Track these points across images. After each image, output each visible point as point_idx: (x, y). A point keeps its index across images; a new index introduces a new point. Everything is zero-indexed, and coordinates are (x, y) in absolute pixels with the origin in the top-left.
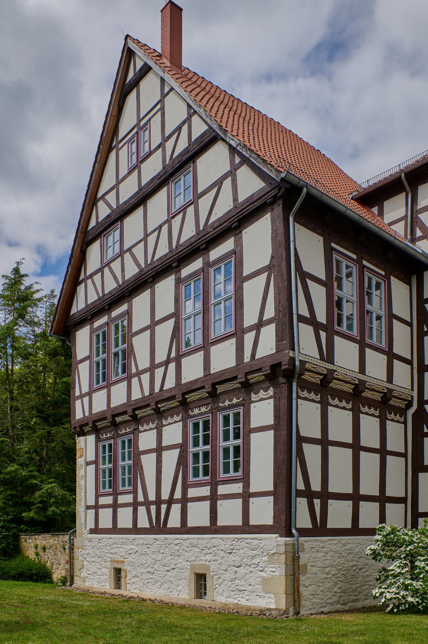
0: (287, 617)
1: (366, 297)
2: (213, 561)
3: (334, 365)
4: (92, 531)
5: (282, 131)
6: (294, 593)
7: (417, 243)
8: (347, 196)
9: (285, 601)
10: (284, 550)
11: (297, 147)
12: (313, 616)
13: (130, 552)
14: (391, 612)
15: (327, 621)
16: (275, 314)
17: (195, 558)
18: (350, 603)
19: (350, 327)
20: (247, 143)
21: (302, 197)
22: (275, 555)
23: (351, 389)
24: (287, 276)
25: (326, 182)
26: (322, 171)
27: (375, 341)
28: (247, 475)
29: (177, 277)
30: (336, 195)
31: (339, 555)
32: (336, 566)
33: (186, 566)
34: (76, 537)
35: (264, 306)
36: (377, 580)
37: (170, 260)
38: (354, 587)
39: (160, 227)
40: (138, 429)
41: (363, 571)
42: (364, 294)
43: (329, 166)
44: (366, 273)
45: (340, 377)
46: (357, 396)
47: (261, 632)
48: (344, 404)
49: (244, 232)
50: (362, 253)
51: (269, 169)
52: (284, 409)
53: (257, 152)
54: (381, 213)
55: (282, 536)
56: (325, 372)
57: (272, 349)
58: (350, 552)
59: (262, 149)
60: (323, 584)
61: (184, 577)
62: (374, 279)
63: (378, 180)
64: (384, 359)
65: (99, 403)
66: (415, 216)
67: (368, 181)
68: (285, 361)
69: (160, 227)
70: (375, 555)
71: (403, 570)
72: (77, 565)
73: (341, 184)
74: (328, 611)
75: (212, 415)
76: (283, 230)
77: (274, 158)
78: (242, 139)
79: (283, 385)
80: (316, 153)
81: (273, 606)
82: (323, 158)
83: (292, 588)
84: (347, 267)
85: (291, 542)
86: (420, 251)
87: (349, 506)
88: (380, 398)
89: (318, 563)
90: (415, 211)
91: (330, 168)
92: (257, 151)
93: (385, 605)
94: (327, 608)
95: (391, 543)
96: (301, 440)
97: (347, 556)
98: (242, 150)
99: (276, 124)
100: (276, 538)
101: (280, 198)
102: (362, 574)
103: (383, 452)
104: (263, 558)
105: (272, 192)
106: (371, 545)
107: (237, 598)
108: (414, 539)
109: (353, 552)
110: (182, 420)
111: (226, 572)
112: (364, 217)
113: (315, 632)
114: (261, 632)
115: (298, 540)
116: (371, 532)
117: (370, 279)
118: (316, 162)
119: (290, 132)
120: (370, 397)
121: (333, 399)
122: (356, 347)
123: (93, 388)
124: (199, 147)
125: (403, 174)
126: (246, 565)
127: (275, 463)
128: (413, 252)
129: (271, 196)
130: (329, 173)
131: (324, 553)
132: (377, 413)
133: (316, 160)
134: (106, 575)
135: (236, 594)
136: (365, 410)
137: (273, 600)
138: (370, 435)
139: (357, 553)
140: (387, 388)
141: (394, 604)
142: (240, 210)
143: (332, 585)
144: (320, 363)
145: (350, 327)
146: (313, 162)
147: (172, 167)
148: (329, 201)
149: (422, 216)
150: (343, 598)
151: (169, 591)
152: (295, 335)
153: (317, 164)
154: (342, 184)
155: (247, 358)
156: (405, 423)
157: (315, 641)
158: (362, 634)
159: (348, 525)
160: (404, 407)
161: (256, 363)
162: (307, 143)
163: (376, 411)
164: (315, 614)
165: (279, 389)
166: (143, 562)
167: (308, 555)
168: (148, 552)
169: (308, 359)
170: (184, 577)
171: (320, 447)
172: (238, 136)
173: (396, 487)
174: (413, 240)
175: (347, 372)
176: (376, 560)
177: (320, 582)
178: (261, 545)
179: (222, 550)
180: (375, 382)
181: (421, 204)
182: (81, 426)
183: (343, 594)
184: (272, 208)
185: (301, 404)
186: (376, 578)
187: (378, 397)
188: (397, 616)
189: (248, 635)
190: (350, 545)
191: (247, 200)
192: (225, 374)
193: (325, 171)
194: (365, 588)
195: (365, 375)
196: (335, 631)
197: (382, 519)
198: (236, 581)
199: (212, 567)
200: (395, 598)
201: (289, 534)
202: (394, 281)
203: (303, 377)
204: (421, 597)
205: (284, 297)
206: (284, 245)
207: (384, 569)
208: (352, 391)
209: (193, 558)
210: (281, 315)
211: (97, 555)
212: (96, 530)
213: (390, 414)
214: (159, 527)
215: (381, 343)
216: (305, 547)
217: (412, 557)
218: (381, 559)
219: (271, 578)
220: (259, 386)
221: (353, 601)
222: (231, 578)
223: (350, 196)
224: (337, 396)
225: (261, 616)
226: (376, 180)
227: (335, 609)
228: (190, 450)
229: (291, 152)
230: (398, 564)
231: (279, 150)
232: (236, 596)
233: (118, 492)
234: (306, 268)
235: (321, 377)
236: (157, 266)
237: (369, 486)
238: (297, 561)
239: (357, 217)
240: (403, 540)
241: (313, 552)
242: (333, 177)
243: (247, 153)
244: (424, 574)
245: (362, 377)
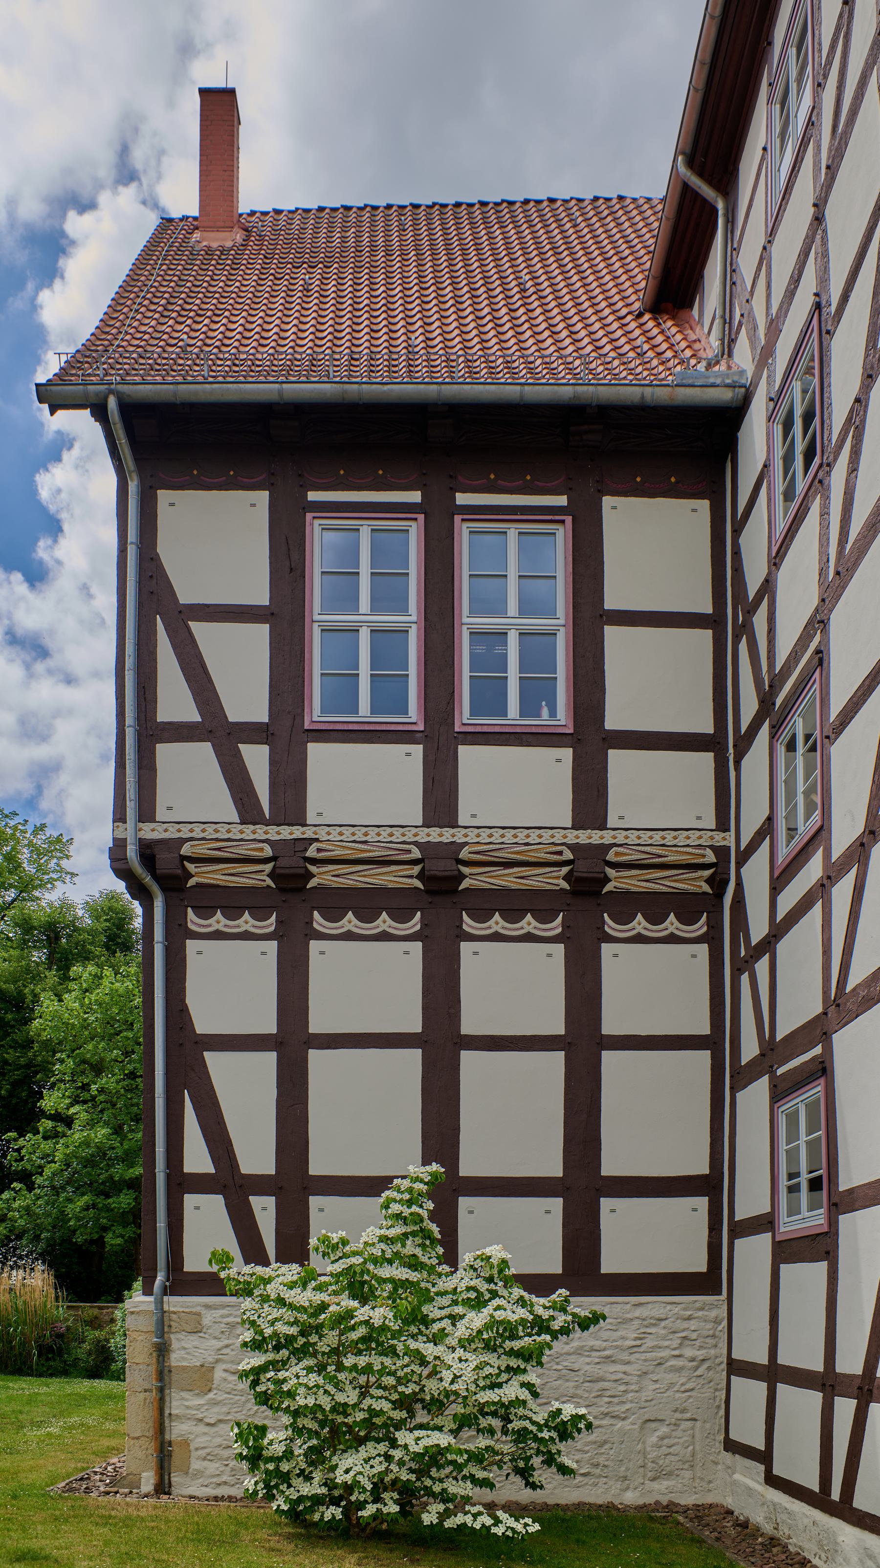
23: (411, 877)
48: (384, 923)
88: (704, 884)
120: (514, 886)
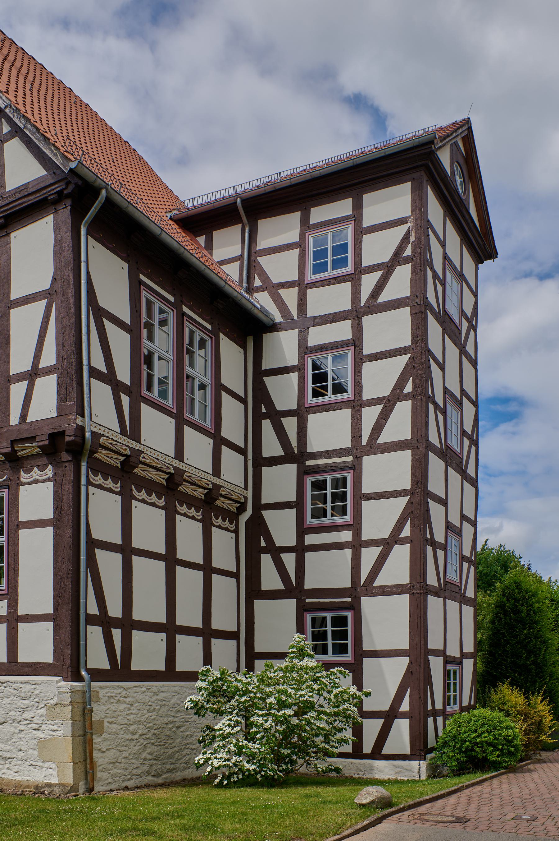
0: (75, 796)
1: (186, 357)
3: (140, 444)
5: (75, 103)
6: (85, 760)
7: (255, 295)
8: (163, 214)
9: (72, 773)
10: (70, 700)
11: (96, 130)
12: (113, 794)
14: (220, 785)
15: (133, 800)
16: (57, 361)
18: (165, 773)
19: (163, 394)
20: (20, 107)
21: (100, 202)
22: (56, 707)
23: (163, 479)
24: (75, 310)
25: (136, 189)
26: (136, 176)
27: (197, 418)
28: (14, 590)
30: (143, 205)
31: (148, 707)
32: (145, 723)
35: (40, 347)
36: (200, 742)
38: (170, 752)
41: (182, 729)
42: (183, 352)
43: (141, 168)
44: (186, 323)
45: (148, 461)
46: (171, 489)
47: (36, 818)
49: (13, 235)
50: (181, 296)
51: (53, 151)
52: (68, 498)
53: (35, 123)
54: (209, 246)
55: (66, 679)
56: (128, 452)
57: (51, 411)
58: (164, 703)
59: (44, 119)
60: (127, 748)
62: (198, 333)
63: (207, 201)
64: (209, 444)
66: (253, 258)
67: (193, 199)
68: (70, 430)
70: (198, 709)
71: (233, 729)
73: (157, 195)
74: (135, 785)
76: (71, 243)
77: (61, 139)
78: (13, 100)
79: (66, 464)
80: (124, 145)
81: (55, 781)
82: (133, 154)
83: (82, 754)
84: (161, 311)
85: (80, 689)
86: (259, 306)
87: (162, 640)
88: (203, 496)
89: (120, 718)
90: (253, 251)
91: (142, 170)
92: (36, 122)
93: (212, 776)
94: (133, 781)
95: (220, 693)
96: (94, 544)
97: (159, 710)
98: (14, 116)
99: (67, 91)
100: (58, 682)
101: (68, 196)
102: (181, 734)
103: (207, 569)
104: (39, 711)
105: (57, 186)
106: (192, 695)
108: (250, 688)
109: (168, 703)
112: (186, 247)
113: (114, 816)
114: (36, 818)
115: (89, 686)
116: (192, 677)
117: (192, 333)
118: (123, 158)
119: (88, 107)
120: (190, 493)
121: (140, 491)
122: (171, 422)
125: (239, 200)
126: (14, 720)
127: (55, 575)
128: (249, 306)
129: (55, 191)
130: (141, 177)
131: (128, 704)
132: (199, 516)
133: (123, 155)
136: (183, 510)
137: (54, 772)
138: (189, 545)
139: (174, 705)
140: (213, 483)
141: (224, 774)
142: (7, 202)
143: (139, 749)
144: (121, 439)
145: (163, 394)
146: (118, 156)
148: (137, 215)
149: (262, 260)
150: (154, 767)
152: (86, 395)
153: (123, 161)
154: (158, 196)
155: (15, 419)
156: (236, 532)
157: (114, 828)
158: (179, 816)
159: (161, 666)
160: (235, 511)
161: (27, 427)
162: (111, 128)
163: (198, 512)
164: (117, 790)
165: (61, 469)
167: (105, 708)
169: (104, 431)
171: (120, 556)
172: (7, 92)
173: (224, 618)
174: (250, 290)
175: (172, 462)
176: (199, 716)
177: (123, 746)
178: (36, 692)
180: (197, 472)
181: (262, 244)
183: (155, 762)
184: (55, 209)
185: (93, 494)
186: (199, 740)
187: (200, 494)
188: (228, 790)
189: (16, 823)
190: (164, 695)
191: (18, 190)
193: (134, 172)
194: (185, 753)
195: (183, 462)
196: (143, 814)
197: (207, 660)
200: (224, 766)
201: (77, 677)
202: (224, 341)
203: (96, 455)
204: (258, 764)
205: (70, 340)
206: (72, 265)
207: (209, 728)
208: (165, 483)
210: (65, 363)
213: (217, 519)
215: (205, 421)
216: (101, 695)
217: (246, 712)
218: (205, 713)
220: (32, 462)
221: (169, 771)
223: (169, 215)
224: (144, 487)
225: (37, 795)
226: (204, 201)
227: (145, 783)
229: (87, 135)
230: (227, 723)
231: (69, 128)
234: (102, 303)
235: (123, 458)
237: (189, 614)
238: (89, 715)
239: (175, 245)
240: (236, 688)
241: (112, 703)
242: (145, 184)
243: (20, 121)
244: (262, 734)
245: (179, 465)
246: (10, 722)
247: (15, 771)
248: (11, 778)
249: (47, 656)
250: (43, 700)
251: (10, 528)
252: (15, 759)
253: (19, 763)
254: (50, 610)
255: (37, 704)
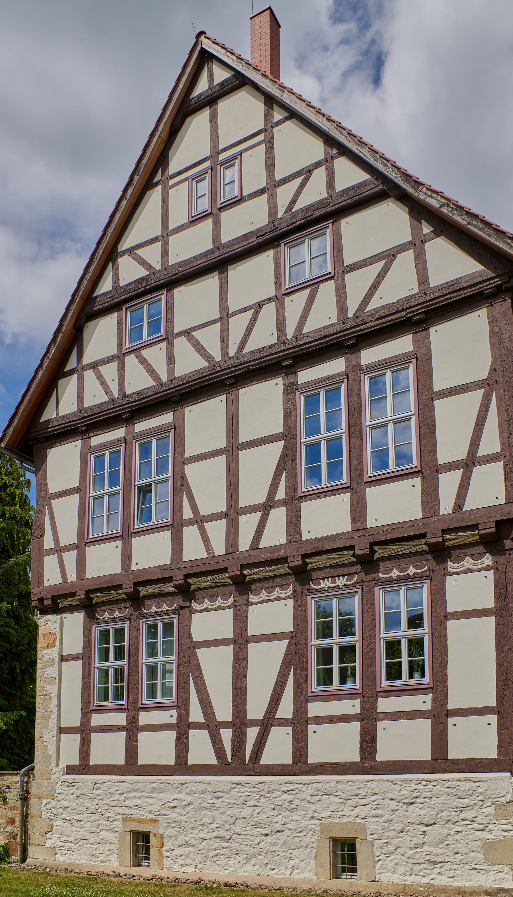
2: (373, 817)
4: (71, 770)
13: (172, 805)
17: (330, 813)
22: (509, 805)
29: (288, 381)
33: (309, 827)
34: (34, 779)
35: (478, 436)
37: (280, 354)
39: (259, 306)
40: (190, 606)
61: (304, 844)
65: (104, 562)
69: (259, 306)
72: (35, 826)
75: (362, 590)
98: (453, 214)
104: (484, 810)
107: (429, 874)
110: (294, 596)
111: (401, 835)
123: (88, 539)
124: (350, 201)
126: (448, 821)
129: (495, 284)
134: (112, 843)
135: (426, 869)
147: (291, 222)
151: (268, 868)
166: (205, 820)
168: (217, 805)
170: (304, 844)
178: (480, 790)
179: (392, 799)
182: (54, 598)
192: (399, 530)
198: (426, 847)
199: (371, 828)
209: (327, 814)
211: (87, 809)
212: (84, 767)
214: (239, 762)
219: (504, 840)
222: (413, 843)
228: (312, 643)
232: (426, 871)
233: (140, 706)
236: (249, 362)
246: (443, 823)
247: (450, 876)
248: (444, 883)
249: (490, 750)
250: (489, 798)
251: (434, 620)
252: (449, 863)
253: (455, 867)
254: (492, 702)
255: (481, 802)
